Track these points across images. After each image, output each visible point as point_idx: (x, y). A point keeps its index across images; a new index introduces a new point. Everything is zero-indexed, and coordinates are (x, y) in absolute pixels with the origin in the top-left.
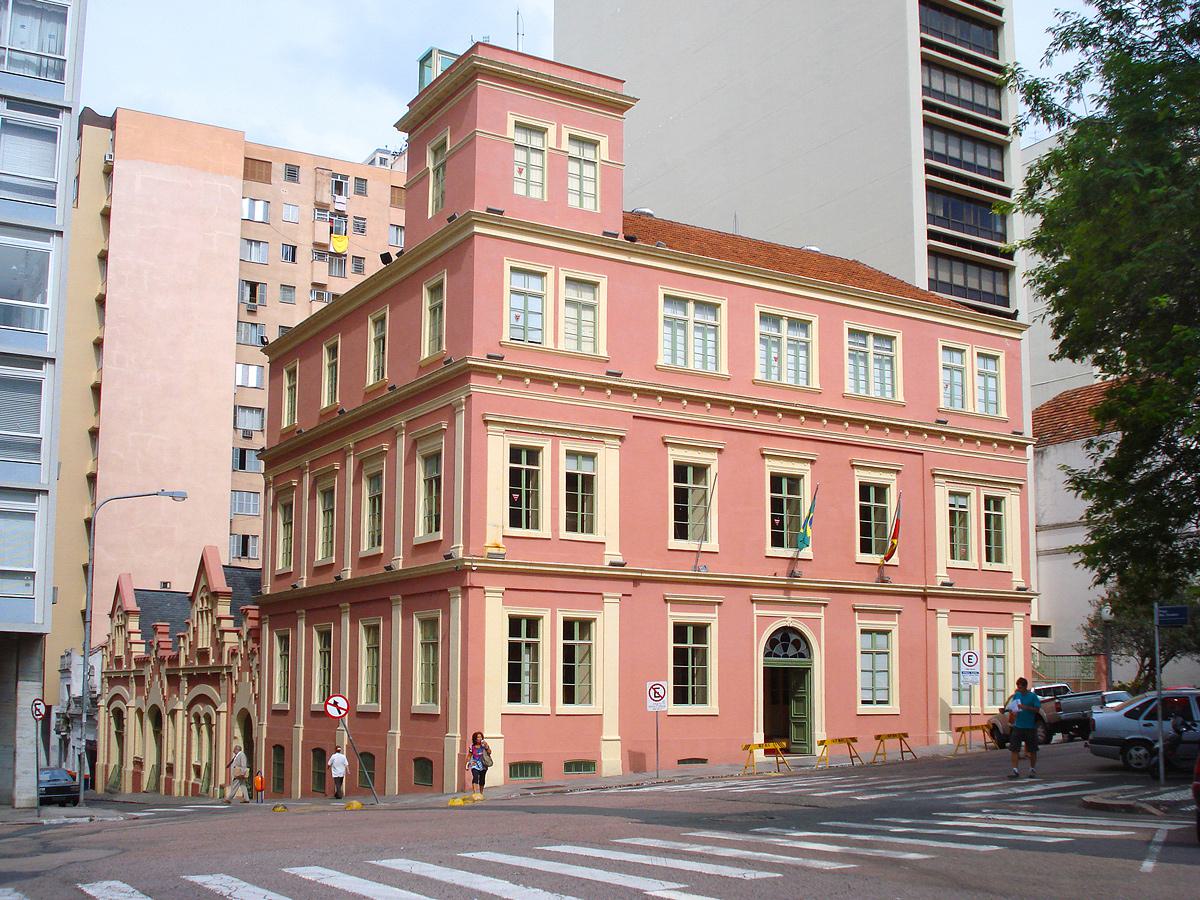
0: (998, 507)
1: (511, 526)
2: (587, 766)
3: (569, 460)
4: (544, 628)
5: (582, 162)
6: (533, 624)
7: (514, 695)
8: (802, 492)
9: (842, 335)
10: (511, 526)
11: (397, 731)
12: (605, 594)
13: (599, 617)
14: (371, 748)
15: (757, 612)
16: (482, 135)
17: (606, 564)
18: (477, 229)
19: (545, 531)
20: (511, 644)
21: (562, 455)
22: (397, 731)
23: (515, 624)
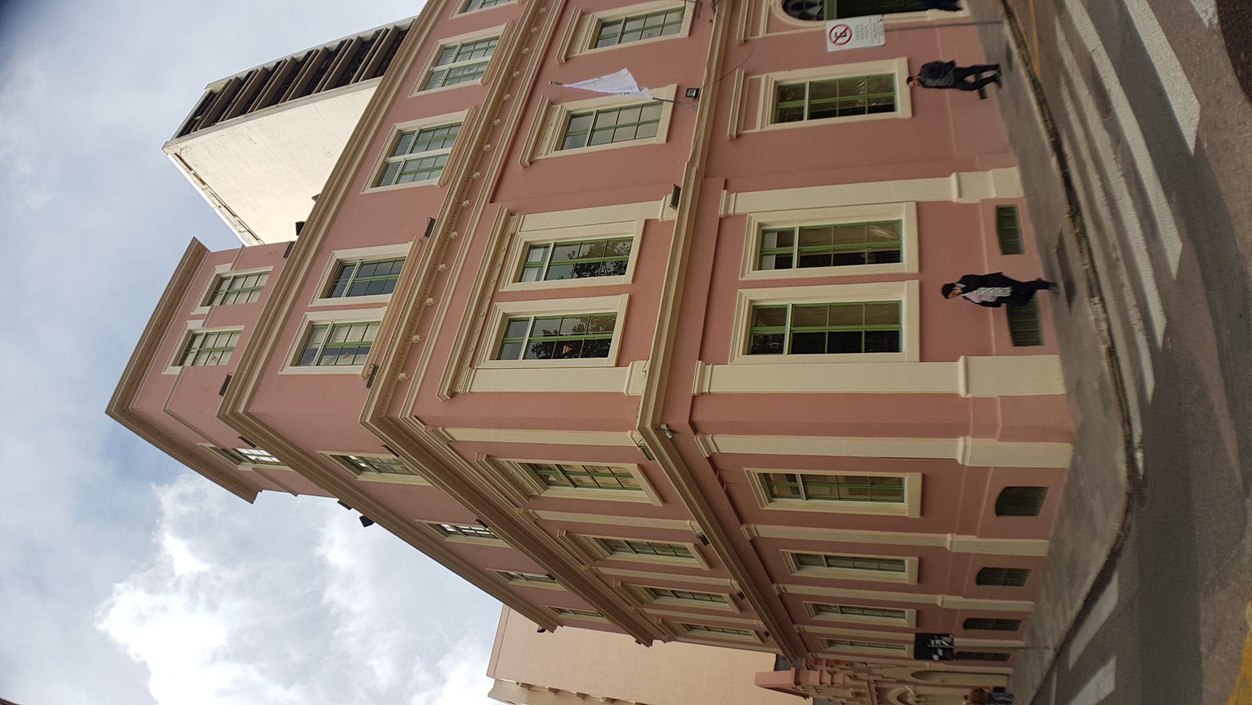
0: (784, 237)
1: (365, 526)
2: (1005, 217)
3: (526, 279)
4: (770, 297)
5: (229, 291)
6: (761, 314)
7: (887, 342)
8: (860, 330)
9: (472, 16)
10: (365, 526)
11: (949, 540)
12: (721, 212)
13: (758, 218)
14: (972, 572)
15: (762, 33)
16: (169, 403)
17: (673, 214)
18: (241, 410)
19: (616, 305)
20: (795, 350)
21: (519, 287)
22: (949, 540)
23: (761, 345)
